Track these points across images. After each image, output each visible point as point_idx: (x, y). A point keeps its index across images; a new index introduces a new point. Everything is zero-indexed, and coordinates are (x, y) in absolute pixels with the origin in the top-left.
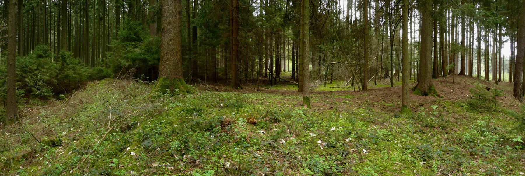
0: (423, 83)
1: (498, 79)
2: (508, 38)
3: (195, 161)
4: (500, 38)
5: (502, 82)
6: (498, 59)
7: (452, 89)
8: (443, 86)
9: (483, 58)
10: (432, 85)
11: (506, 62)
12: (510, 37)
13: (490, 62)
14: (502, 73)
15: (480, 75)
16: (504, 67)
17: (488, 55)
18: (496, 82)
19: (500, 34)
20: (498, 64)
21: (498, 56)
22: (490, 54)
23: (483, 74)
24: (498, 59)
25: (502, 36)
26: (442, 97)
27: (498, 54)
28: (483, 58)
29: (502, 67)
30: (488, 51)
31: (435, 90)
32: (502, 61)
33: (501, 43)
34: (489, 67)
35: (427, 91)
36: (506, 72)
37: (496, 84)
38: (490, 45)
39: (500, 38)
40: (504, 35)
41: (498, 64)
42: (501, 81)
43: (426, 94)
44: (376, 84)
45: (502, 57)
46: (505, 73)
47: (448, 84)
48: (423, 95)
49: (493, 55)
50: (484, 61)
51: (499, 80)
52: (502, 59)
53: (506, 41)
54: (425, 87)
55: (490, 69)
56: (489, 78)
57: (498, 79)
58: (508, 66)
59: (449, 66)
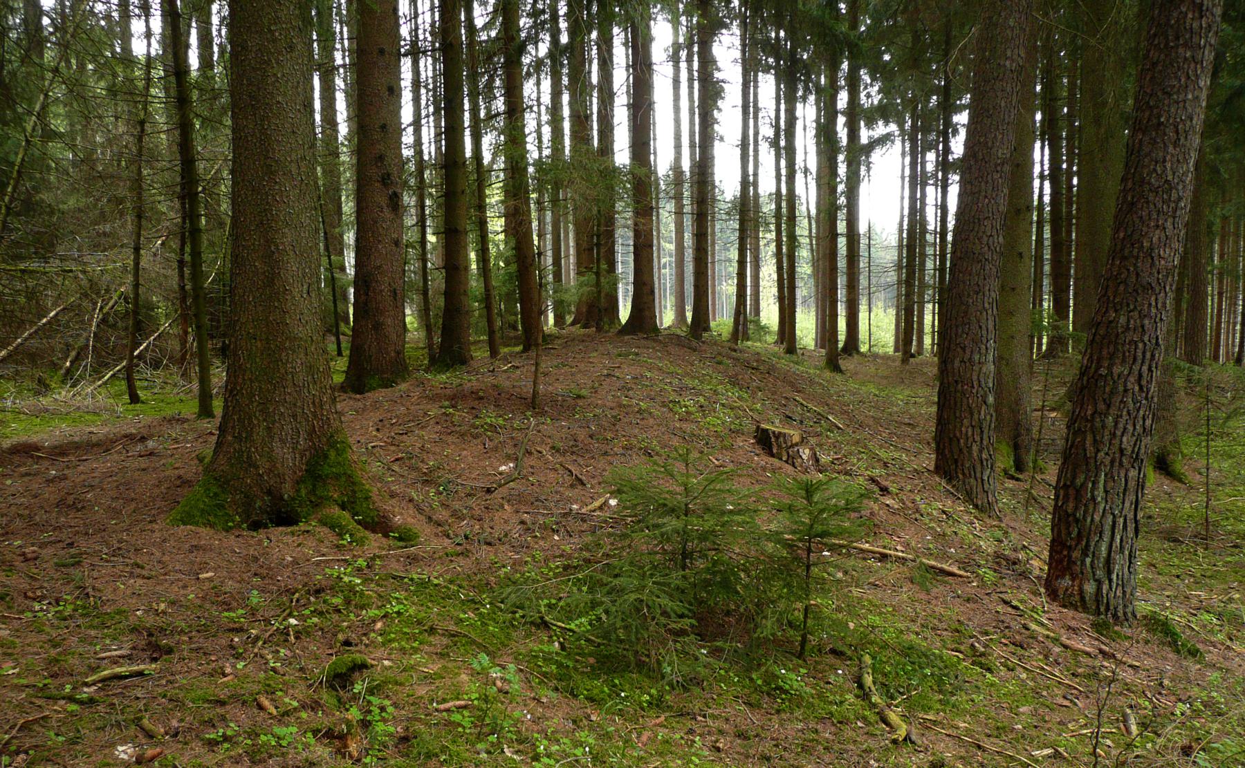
0: (260, 432)
1: (841, 345)
2: (893, 127)
3: (1143, 135)
4: (853, 134)
5: (862, 355)
6: (842, 242)
7: (509, 458)
8: (449, 428)
9: (767, 240)
10: (332, 444)
11: (882, 254)
12: (901, 125)
13: (804, 253)
14: (863, 308)
15: (757, 322)
16: (874, 281)
17: (792, 218)
18: (833, 364)
19: (855, 114)
20: (842, 263)
21: (842, 227)
22: (801, 209)
23: (770, 314)
24: (842, 242)
25: (760, 74)
26: (406, 538)
27: (842, 215)
28: (767, 240)
29: (863, 282)
30: (792, 197)
31: (351, 481)
32: (863, 250)
33: (859, 154)
34: (799, 283)
35: (287, 491)
36: (880, 304)
37: (828, 374)
38: (806, 171)
39: (853, 134)
40: (872, 117)
41: (842, 263)
42: (857, 349)
43: (285, 517)
44: (134, 399)
45: (862, 228)
46: (874, 309)
47: (490, 416)
48: (255, 526)
49: (817, 222)
50: (94, 439)
51: (845, 349)
52: (863, 242)
53: (884, 140)
54: (271, 459)
55: (805, 289)
56: (798, 333)
57: (841, 345)
58: (892, 277)
59: (581, 285)
